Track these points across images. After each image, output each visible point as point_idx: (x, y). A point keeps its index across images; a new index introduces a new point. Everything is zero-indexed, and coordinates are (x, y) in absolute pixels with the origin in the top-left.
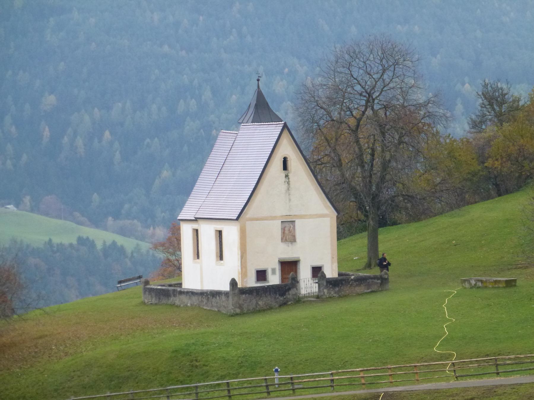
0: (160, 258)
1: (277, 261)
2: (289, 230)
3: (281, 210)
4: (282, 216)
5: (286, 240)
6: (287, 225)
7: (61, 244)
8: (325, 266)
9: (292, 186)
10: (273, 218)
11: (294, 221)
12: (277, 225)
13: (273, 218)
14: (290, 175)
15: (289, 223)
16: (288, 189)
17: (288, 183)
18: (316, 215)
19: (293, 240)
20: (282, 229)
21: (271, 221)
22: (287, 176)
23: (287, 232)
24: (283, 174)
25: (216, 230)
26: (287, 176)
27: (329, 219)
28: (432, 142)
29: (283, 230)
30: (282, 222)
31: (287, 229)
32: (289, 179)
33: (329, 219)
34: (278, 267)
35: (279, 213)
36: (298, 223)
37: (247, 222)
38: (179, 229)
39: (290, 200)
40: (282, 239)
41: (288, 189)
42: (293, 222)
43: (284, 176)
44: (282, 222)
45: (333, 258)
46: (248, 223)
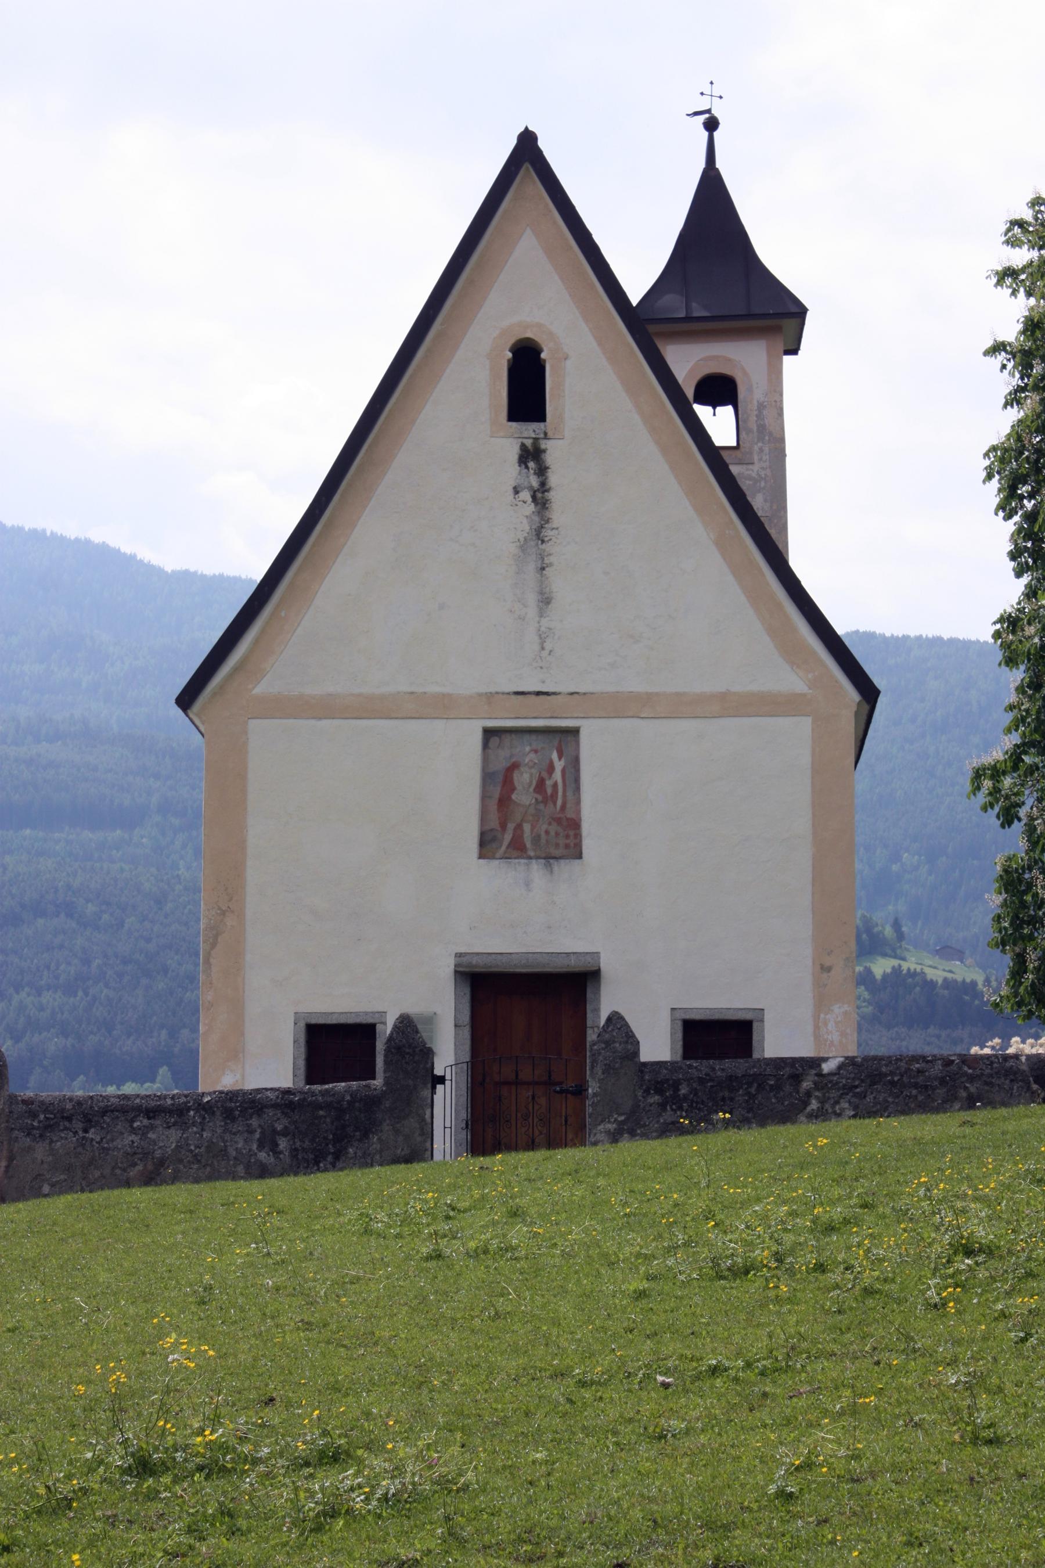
1: (446, 969)
2: (541, 783)
3: (487, 658)
4: (490, 697)
5: (518, 849)
6: (525, 751)
8: (768, 1017)
9: (558, 515)
10: (441, 707)
11: (575, 732)
13: (441, 707)
14: (554, 453)
15: (538, 742)
16: (539, 534)
17: (541, 498)
18: (723, 697)
20: (487, 777)
21: (413, 725)
22: (531, 456)
23: (523, 796)
24: (507, 442)
25: (481, 856)
26: (531, 456)
27: (805, 724)
30: (489, 733)
31: (524, 779)
32: (542, 471)
33: (805, 724)
35: (466, 680)
36: (596, 742)
37: (253, 724)
38: (771, 1059)
39: (545, 600)
41: (539, 534)
42: (575, 732)
43: (513, 452)
44: (489, 733)
45: (826, 969)
46: (261, 732)
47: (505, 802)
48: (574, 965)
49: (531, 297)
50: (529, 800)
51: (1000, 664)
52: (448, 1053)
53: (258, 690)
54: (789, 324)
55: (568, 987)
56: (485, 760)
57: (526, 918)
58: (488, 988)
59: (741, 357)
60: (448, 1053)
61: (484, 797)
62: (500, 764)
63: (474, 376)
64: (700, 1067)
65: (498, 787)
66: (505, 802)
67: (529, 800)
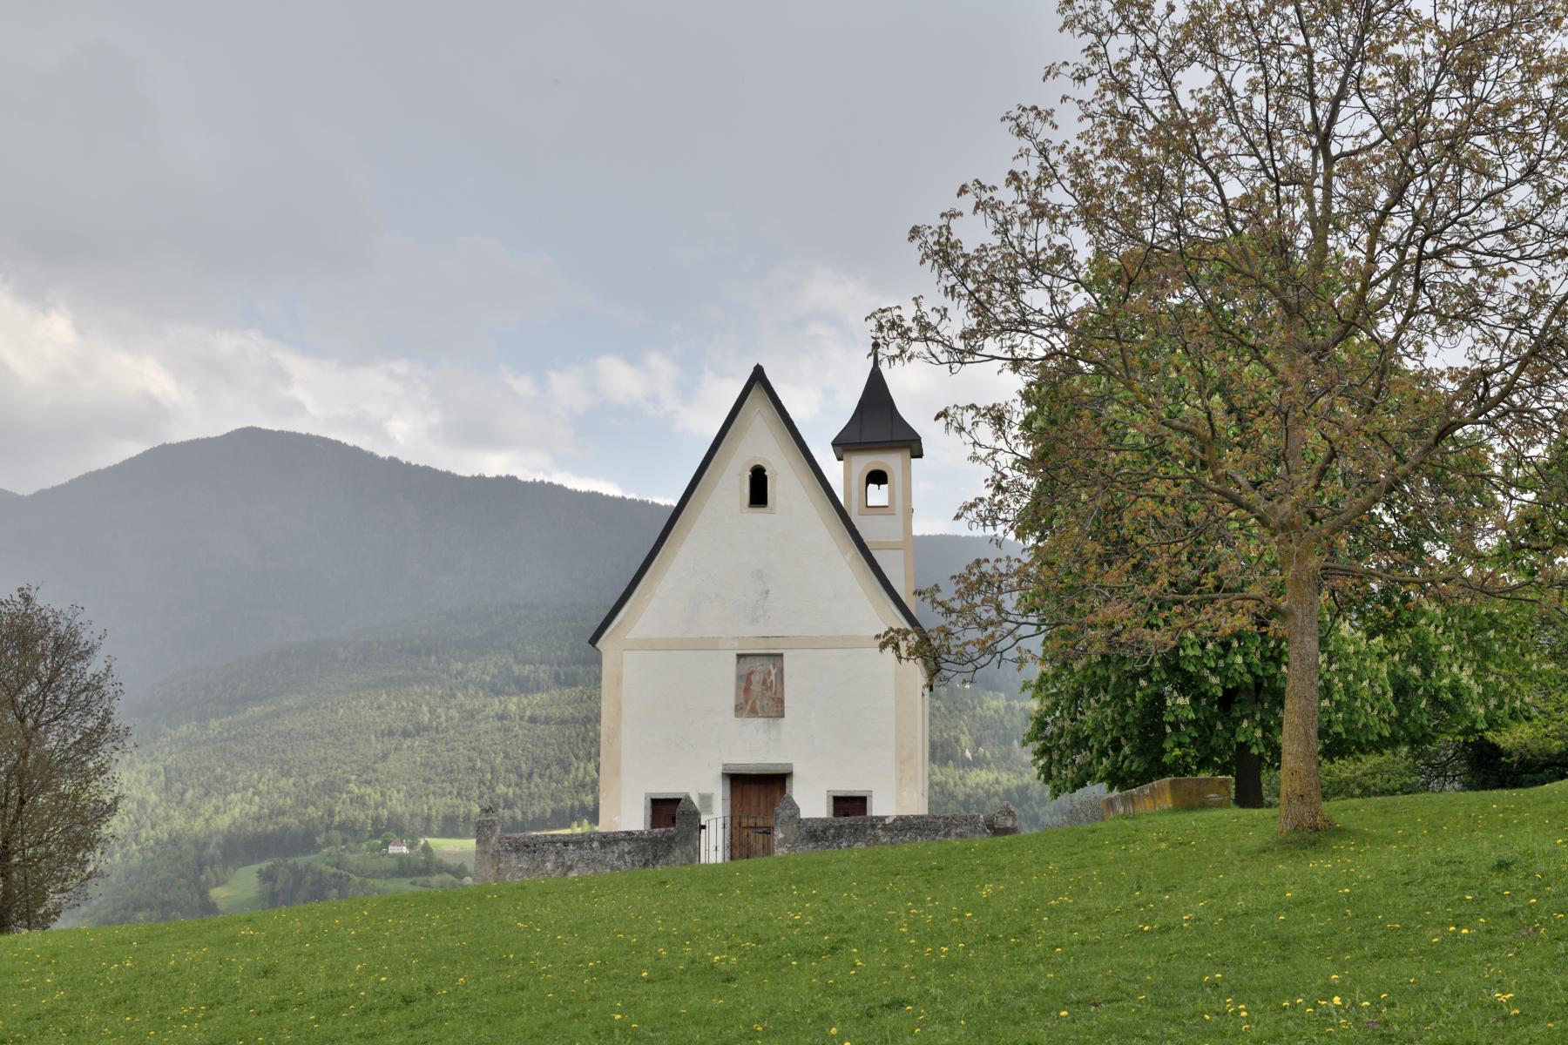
0: (1446, 391)
1: (719, 771)
2: (765, 681)
5: (754, 712)
6: (756, 665)
7: (67, 649)
10: (707, 645)
11: (781, 655)
12: (728, 671)
13: (707, 645)
15: (765, 661)
19: (777, 709)
20: (739, 678)
23: (756, 687)
28: (1504, 641)
29: (745, 682)
30: (740, 656)
31: (756, 678)
34: (719, 794)
40: (739, 710)
42: (781, 655)
44: (740, 656)
47: (747, 690)
48: (780, 771)
49: (759, 444)
50: (760, 685)
51: (878, 637)
52: (264, 865)
53: (630, 636)
54: (915, 445)
55: (775, 782)
56: (738, 670)
57: (756, 749)
58: (739, 782)
59: (889, 461)
60: (264, 865)
61: (738, 687)
62: (744, 672)
63: (732, 483)
64: (845, 820)
65: (745, 682)
66: (747, 690)
67: (760, 685)
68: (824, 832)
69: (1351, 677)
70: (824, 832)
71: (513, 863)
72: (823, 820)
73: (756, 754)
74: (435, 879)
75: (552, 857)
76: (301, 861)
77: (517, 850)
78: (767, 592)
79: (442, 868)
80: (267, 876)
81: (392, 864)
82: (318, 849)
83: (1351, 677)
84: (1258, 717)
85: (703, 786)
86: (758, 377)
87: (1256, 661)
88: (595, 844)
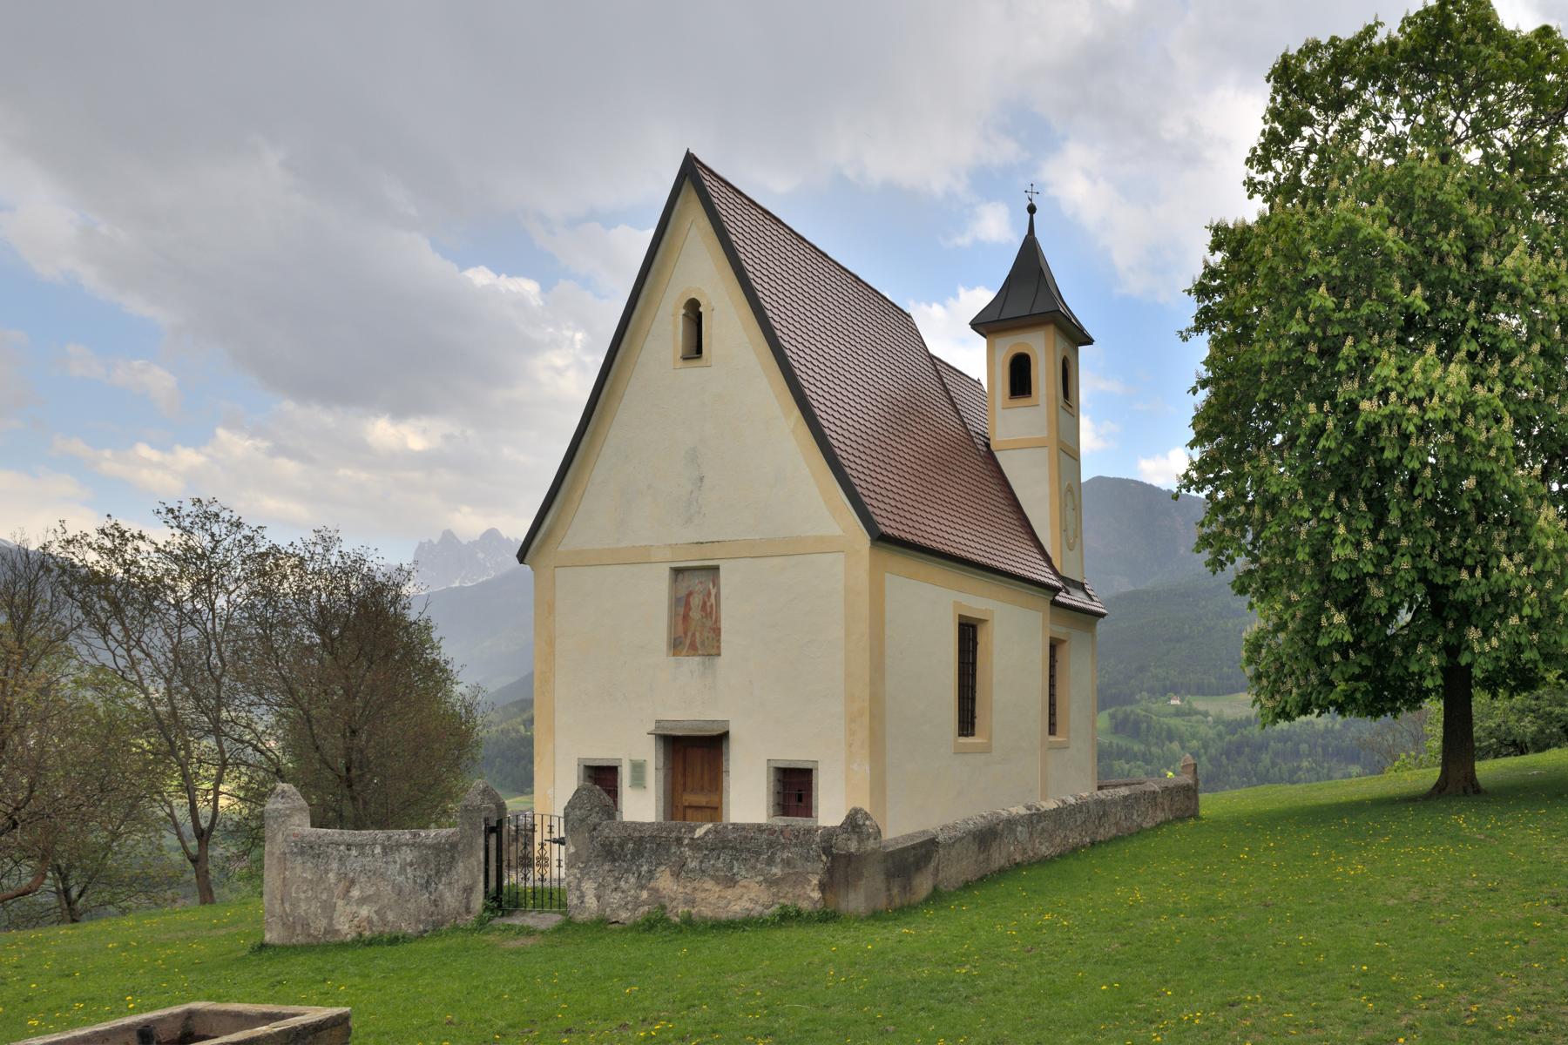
11: (716, 568)
13: (639, 557)
30: (677, 572)
31: (696, 601)
42: (716, 568)
44: (677, 572)
47: (686, 617)
60: (1111, 711)
62: (683, 593)
68: (621, 846)
69: (1549, 584)
70: (621, 846)
71: (298, 871)
72: (651, 824)
73: (691, 710)
74: (1194, 718)
75: (335, 865)
76: (1128, 708)
77: (302, 853)
78: (702, 479)
79: (1197, 713)
80: (1113, 717)
81: (1173, 710)
82: (1138, 702)
83: (1549, 584)
84: (1440, 640)
85: (636, 751)
86: (691, 171)
87: (1430, 565)
88: (378, 850)
